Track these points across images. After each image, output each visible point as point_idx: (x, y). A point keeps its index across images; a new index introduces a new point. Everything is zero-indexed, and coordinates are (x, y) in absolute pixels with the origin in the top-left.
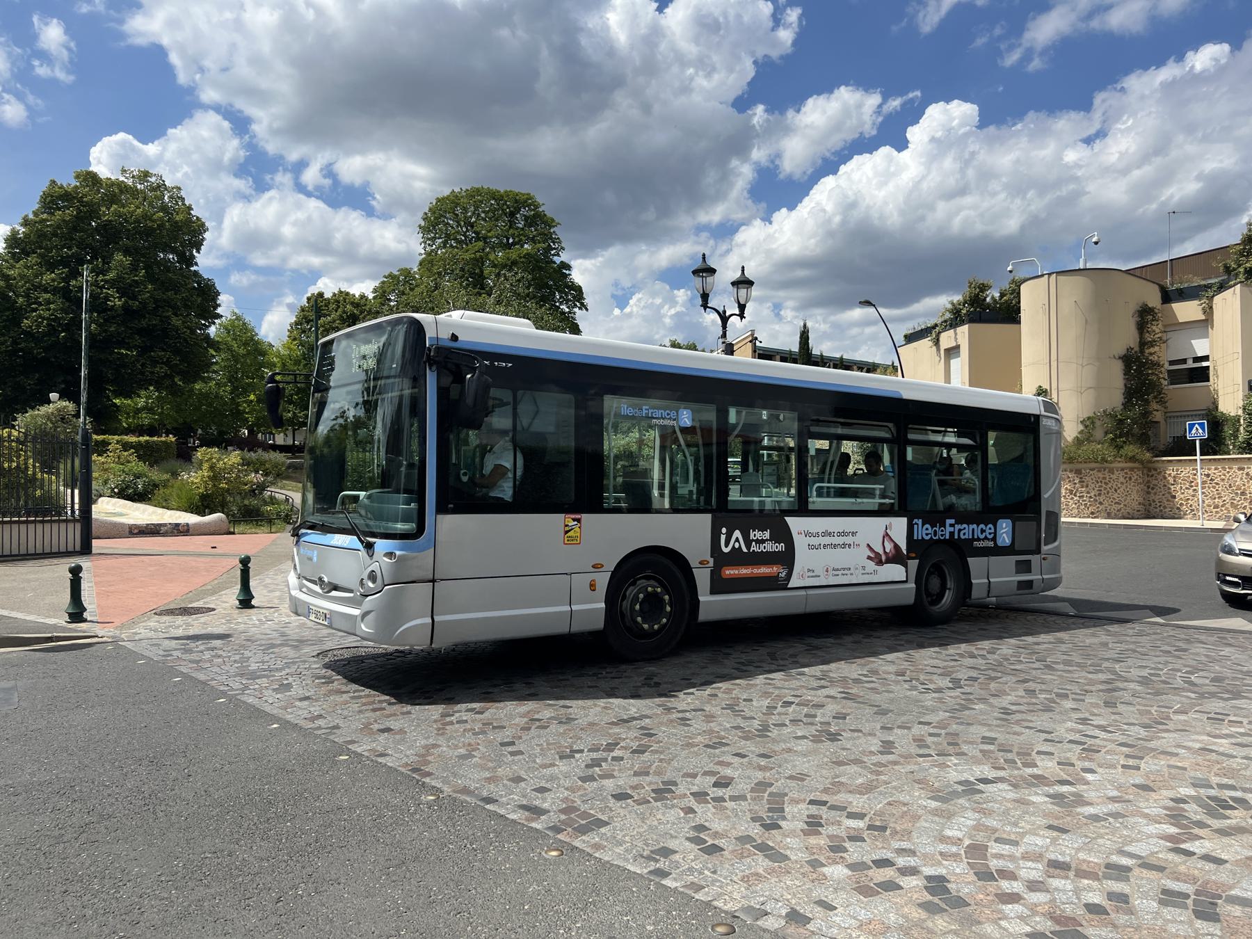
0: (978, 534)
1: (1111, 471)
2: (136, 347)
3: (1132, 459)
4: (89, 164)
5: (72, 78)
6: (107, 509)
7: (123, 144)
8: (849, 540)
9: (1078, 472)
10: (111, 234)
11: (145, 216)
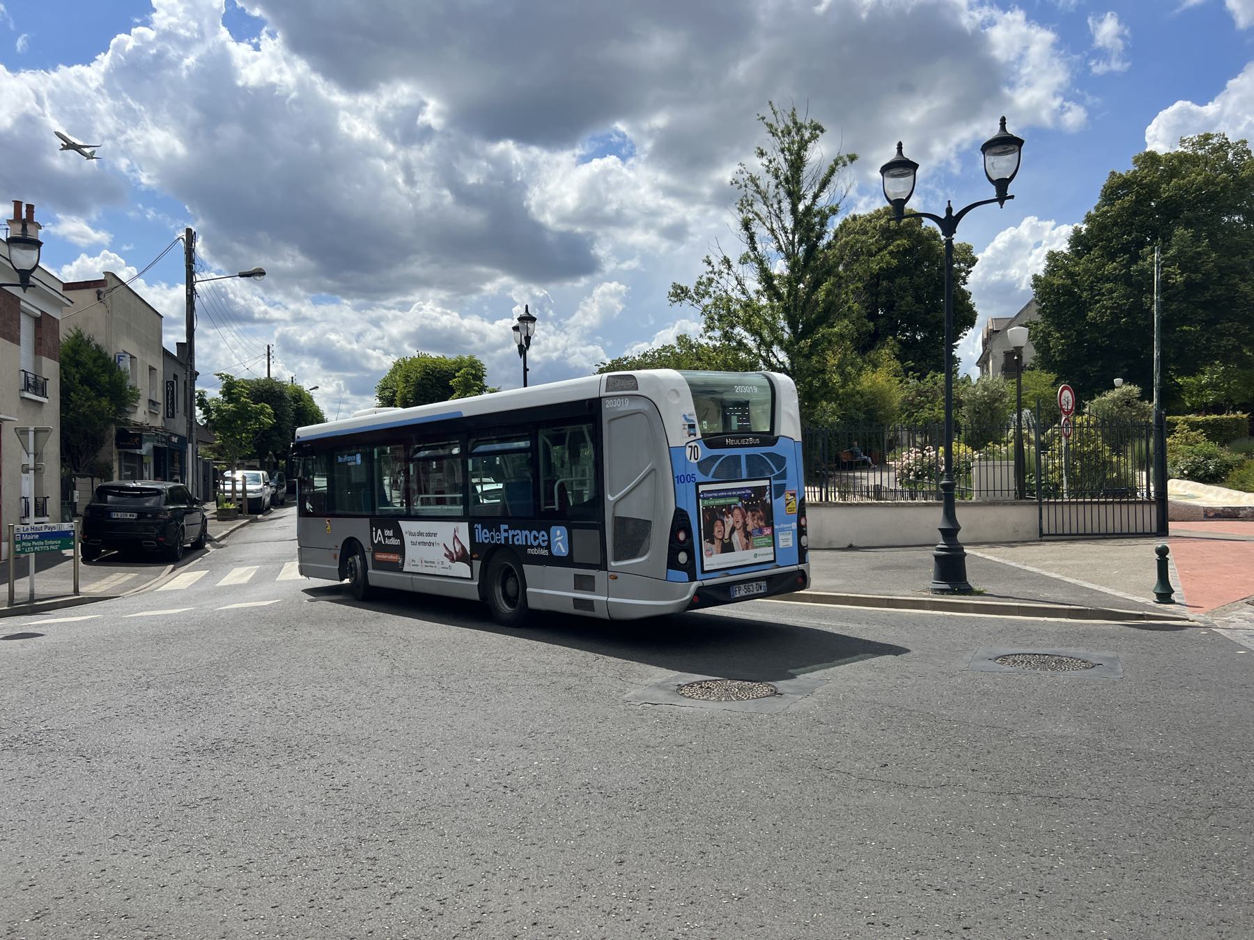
0: (531, 540)
2: (1199, 322)
4: (1145, 145)
5: (1127, 65)
6: (1180, 490)
7: (1181, 113)
8: (432, 539)
10: (1172, 210)
11: (1208, 182)
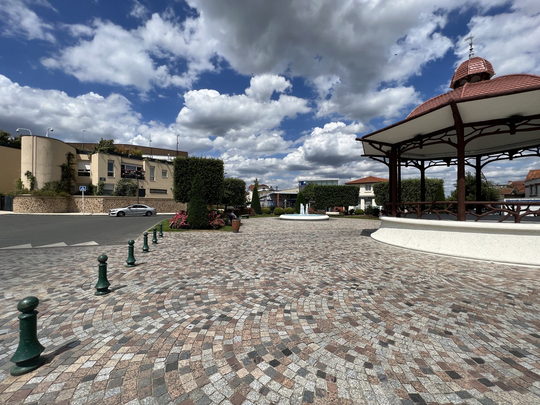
1: (56, 199)
3: (63, 196)
9: (43, 199)
